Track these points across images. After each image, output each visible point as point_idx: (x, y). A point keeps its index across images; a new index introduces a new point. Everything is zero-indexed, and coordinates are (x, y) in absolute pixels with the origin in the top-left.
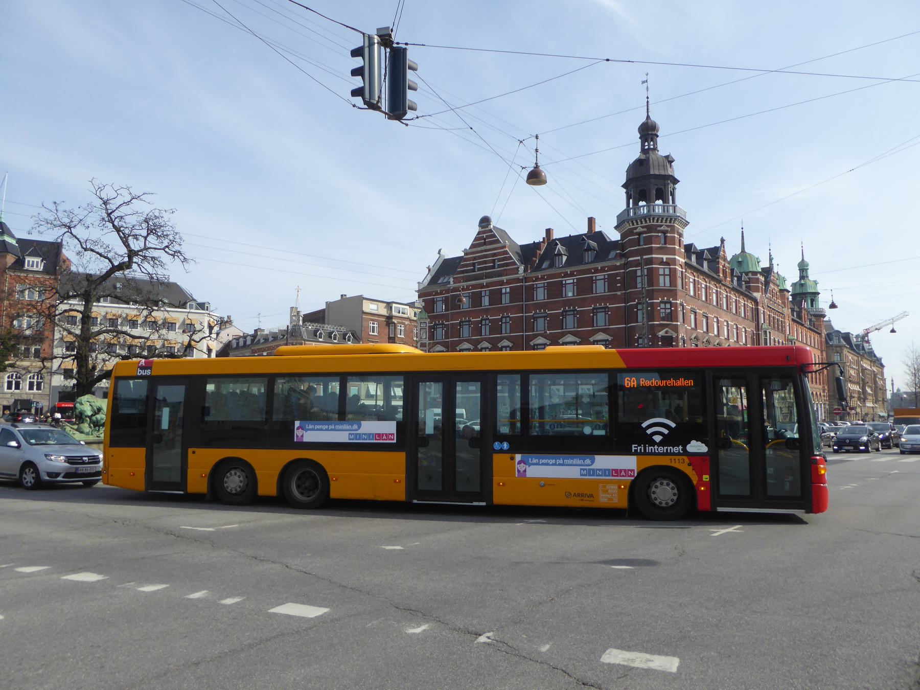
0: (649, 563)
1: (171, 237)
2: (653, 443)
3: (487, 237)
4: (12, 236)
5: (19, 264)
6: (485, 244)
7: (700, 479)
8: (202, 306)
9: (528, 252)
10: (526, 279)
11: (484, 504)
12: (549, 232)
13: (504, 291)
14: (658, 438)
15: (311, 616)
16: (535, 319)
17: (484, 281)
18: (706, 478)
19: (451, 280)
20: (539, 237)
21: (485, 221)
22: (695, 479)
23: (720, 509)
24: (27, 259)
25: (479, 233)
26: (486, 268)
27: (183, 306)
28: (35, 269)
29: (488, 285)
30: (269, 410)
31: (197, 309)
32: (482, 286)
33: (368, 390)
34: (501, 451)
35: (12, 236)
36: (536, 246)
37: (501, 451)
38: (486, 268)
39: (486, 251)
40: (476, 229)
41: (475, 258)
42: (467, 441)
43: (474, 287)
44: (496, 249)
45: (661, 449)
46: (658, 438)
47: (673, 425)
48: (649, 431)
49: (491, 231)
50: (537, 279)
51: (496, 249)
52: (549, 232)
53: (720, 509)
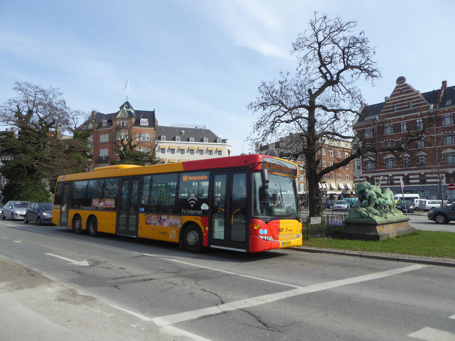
0: (151, 279)
1: (31, 106)
2: (190, 208)
3: (403, 89)
4: (132, 109)
5: (137, 123)
6: (401, 94)
7: (205, 229)
8: (224, 141)
9: (432, 96)
10: (435, 113)
11: (244, 251)
12: (444, 83)
13: (418, 121)
14: (192, 206)
15: (428, 329)
16: (444, 137)
17: (403, 116)
18: (207, 228)
19: (377, 117)
20: (438, 86)
21: (401, 80)
22: (203, 228)
23: (212, 246)
24: (141, 120)
25: (397, 87)
26: (404, 108)
27: (215, 141)
28: (145, 125)
29: (405, 119)
30: (86, 196)
31: (222, 143)
32: (401, 119)
33: (331, 186)
34: (142, 212)
35: (132, 109)
36: (438, 92)
37: (142, 212)
38: (404, 108)
39: (403, 97)
40: (394, 85)
41: (394, 103)
42: (427, 217)
43: (394, 120)
44: (411, 96)
45: (193, 212)
46: (192, 206)
47: (197, 200)
48: (190, 203)
49: (406, 85)
50: (445, 112)
51: (411, 96)
52: (444, 83)
53: (212, 246)
